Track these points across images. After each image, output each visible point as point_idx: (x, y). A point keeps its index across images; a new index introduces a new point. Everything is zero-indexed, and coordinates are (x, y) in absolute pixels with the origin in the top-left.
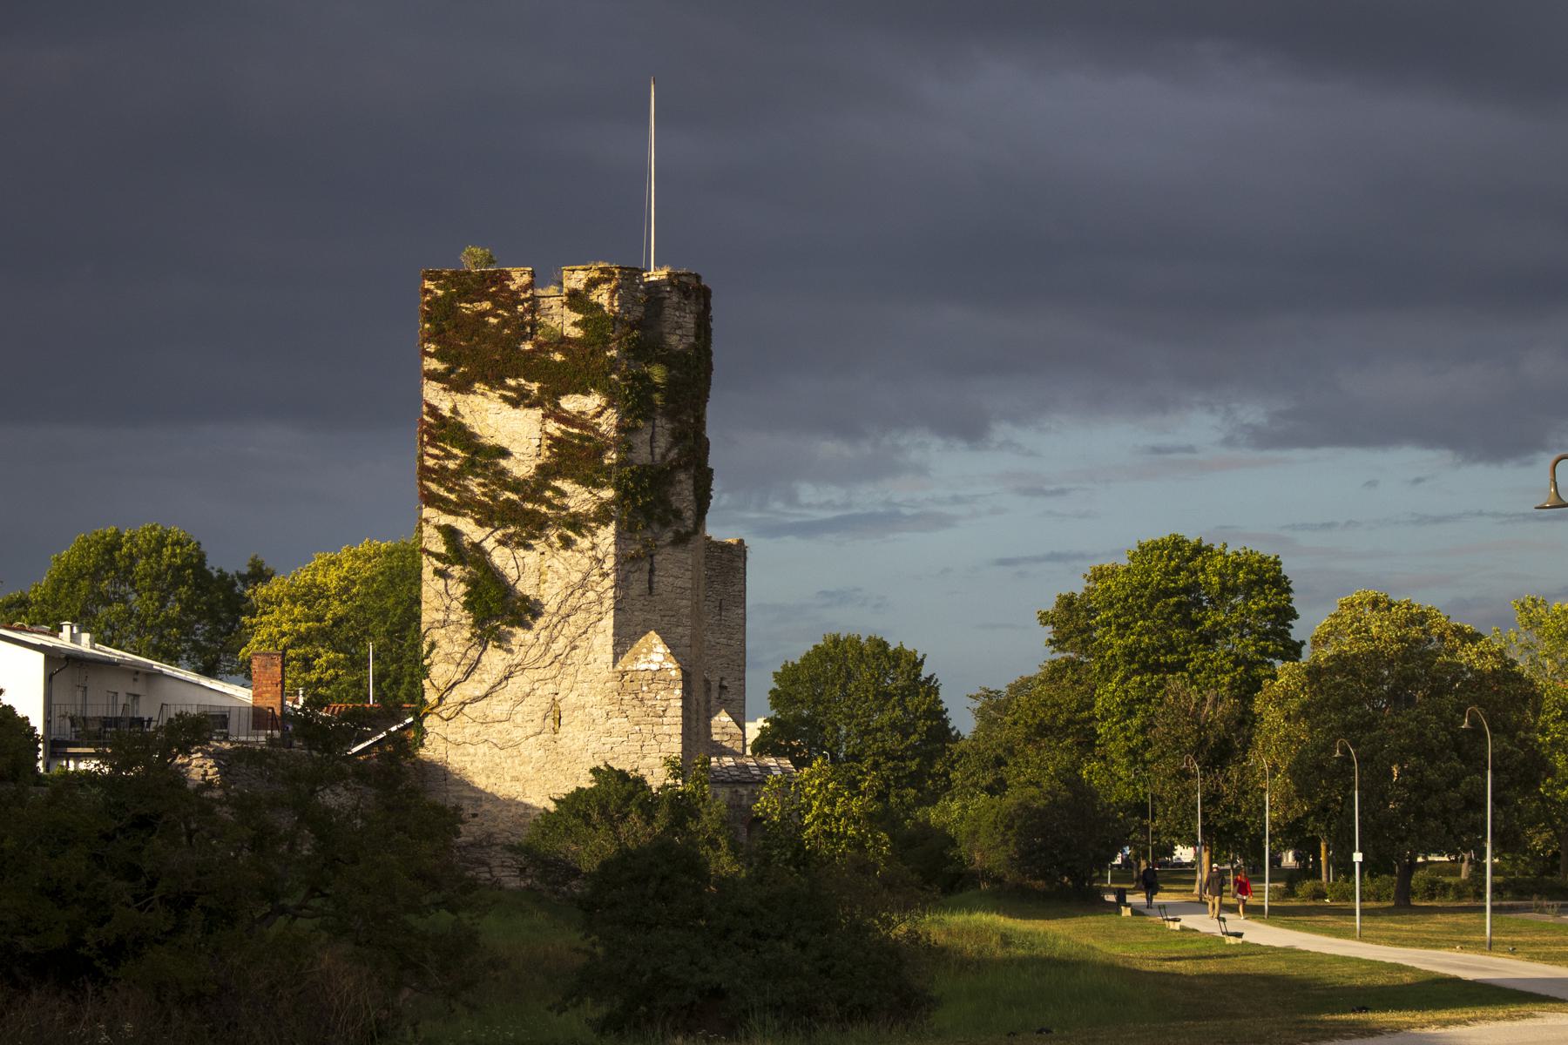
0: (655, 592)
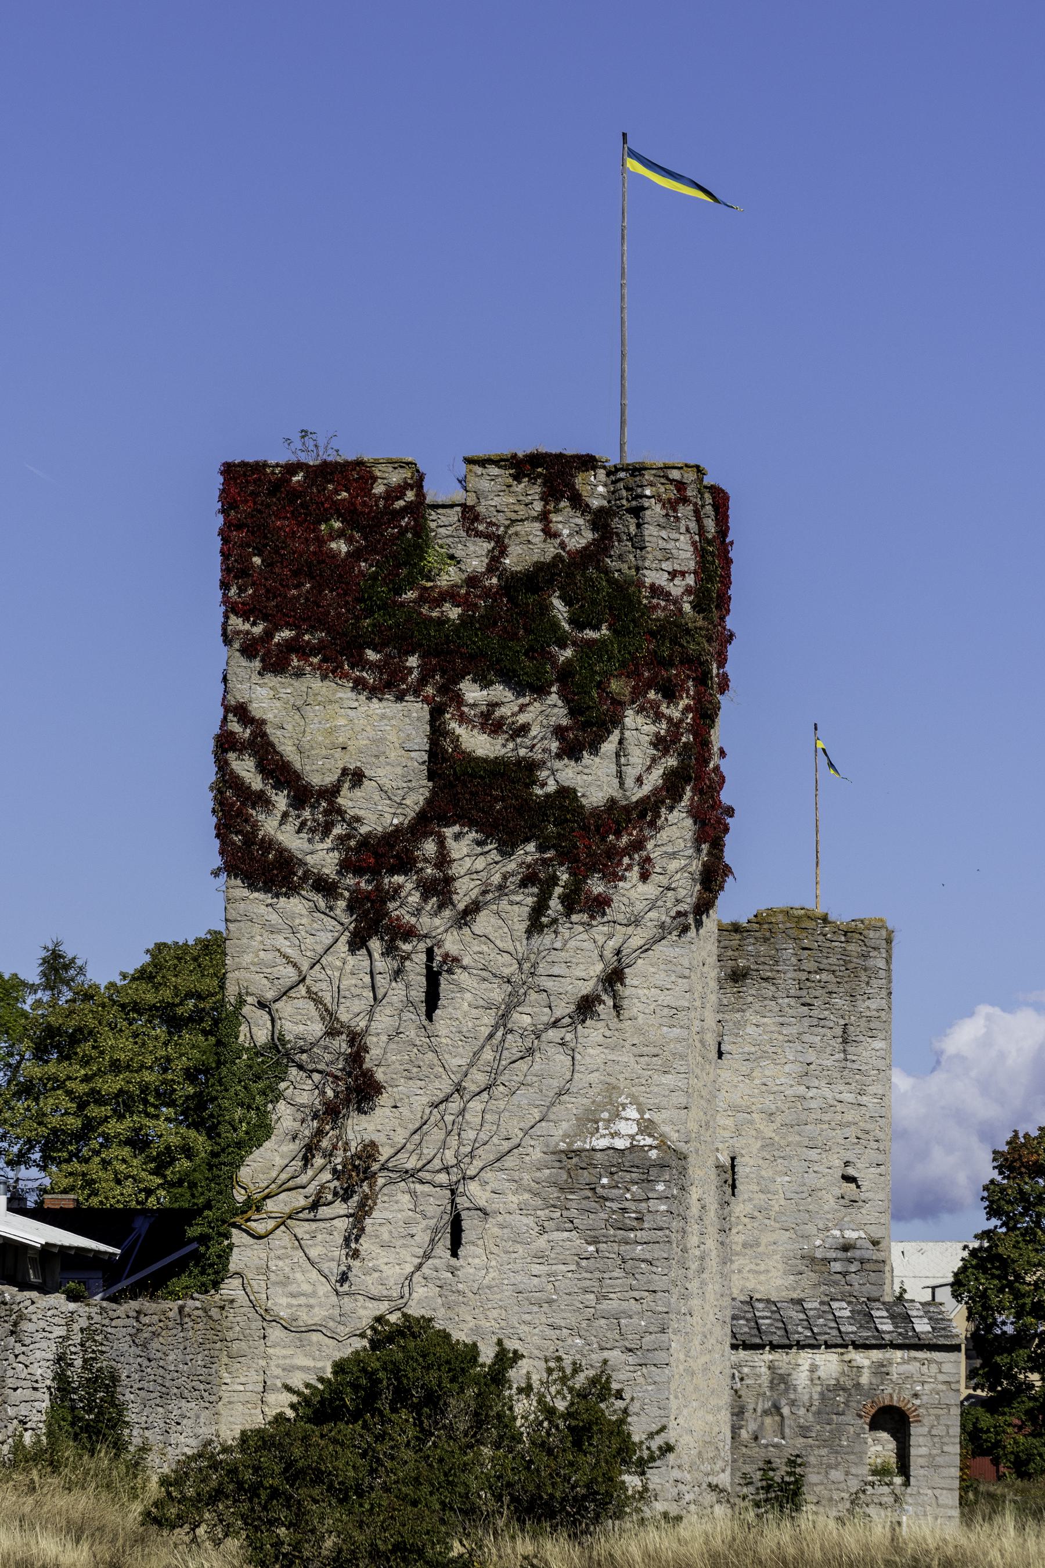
0: (625, 1014)
